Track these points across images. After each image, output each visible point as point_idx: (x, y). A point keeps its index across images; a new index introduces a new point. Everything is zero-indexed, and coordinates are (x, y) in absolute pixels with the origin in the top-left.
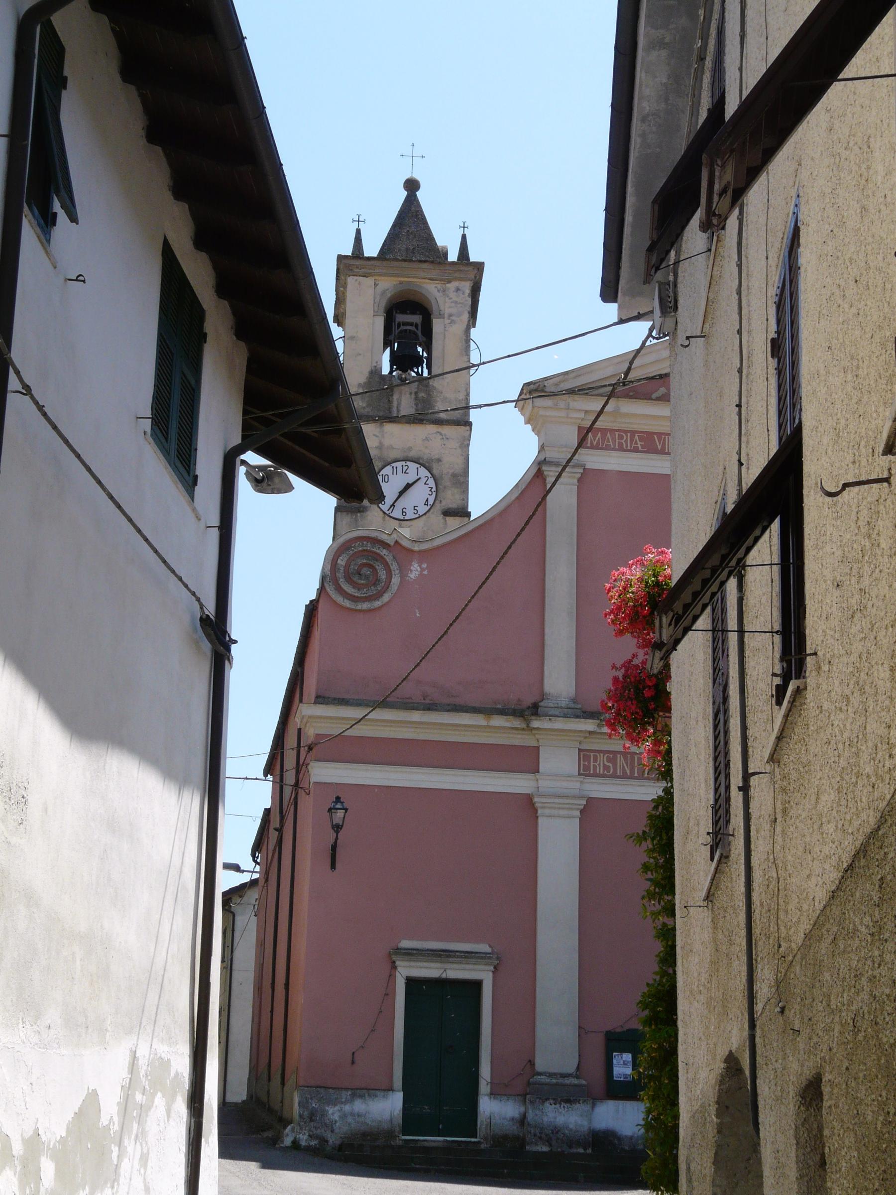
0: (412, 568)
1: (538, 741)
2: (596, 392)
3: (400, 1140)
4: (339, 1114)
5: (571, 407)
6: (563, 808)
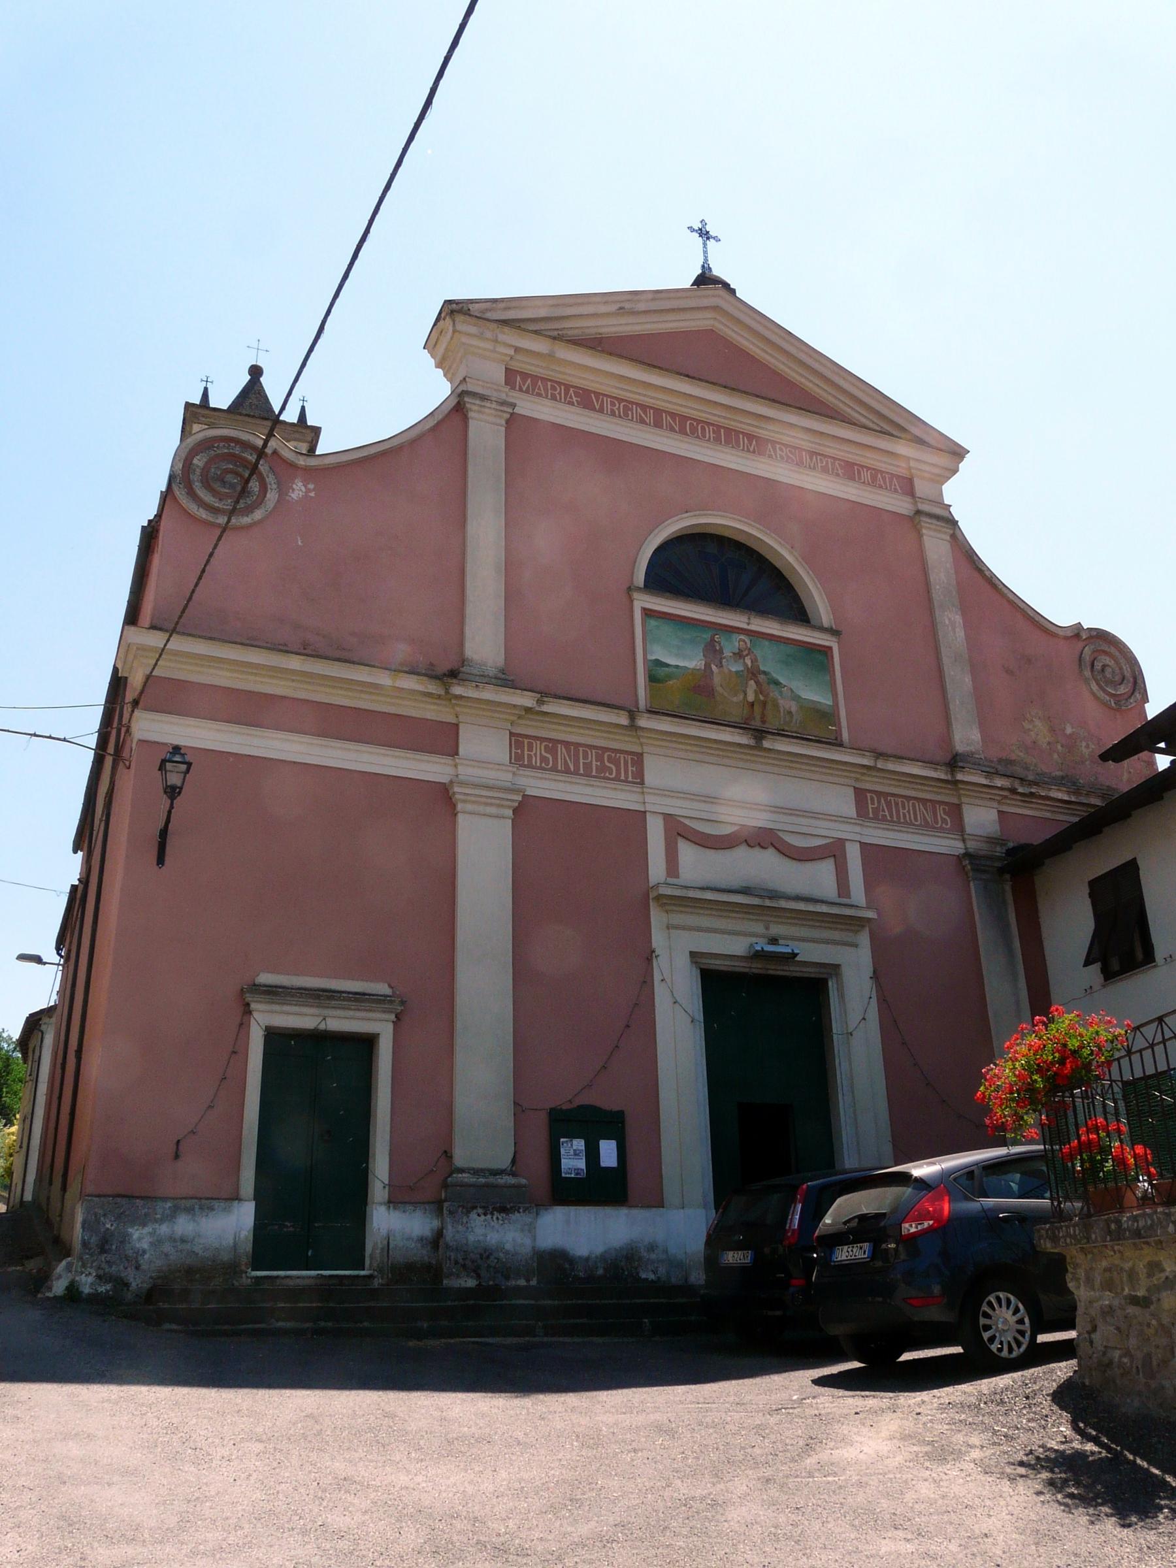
0: (294, 486)
1: (457, 717)
2: (532, 327)
3: (247, 1277)
4: (151, 1240)
5: (499, 340)
6: (491, 805)
